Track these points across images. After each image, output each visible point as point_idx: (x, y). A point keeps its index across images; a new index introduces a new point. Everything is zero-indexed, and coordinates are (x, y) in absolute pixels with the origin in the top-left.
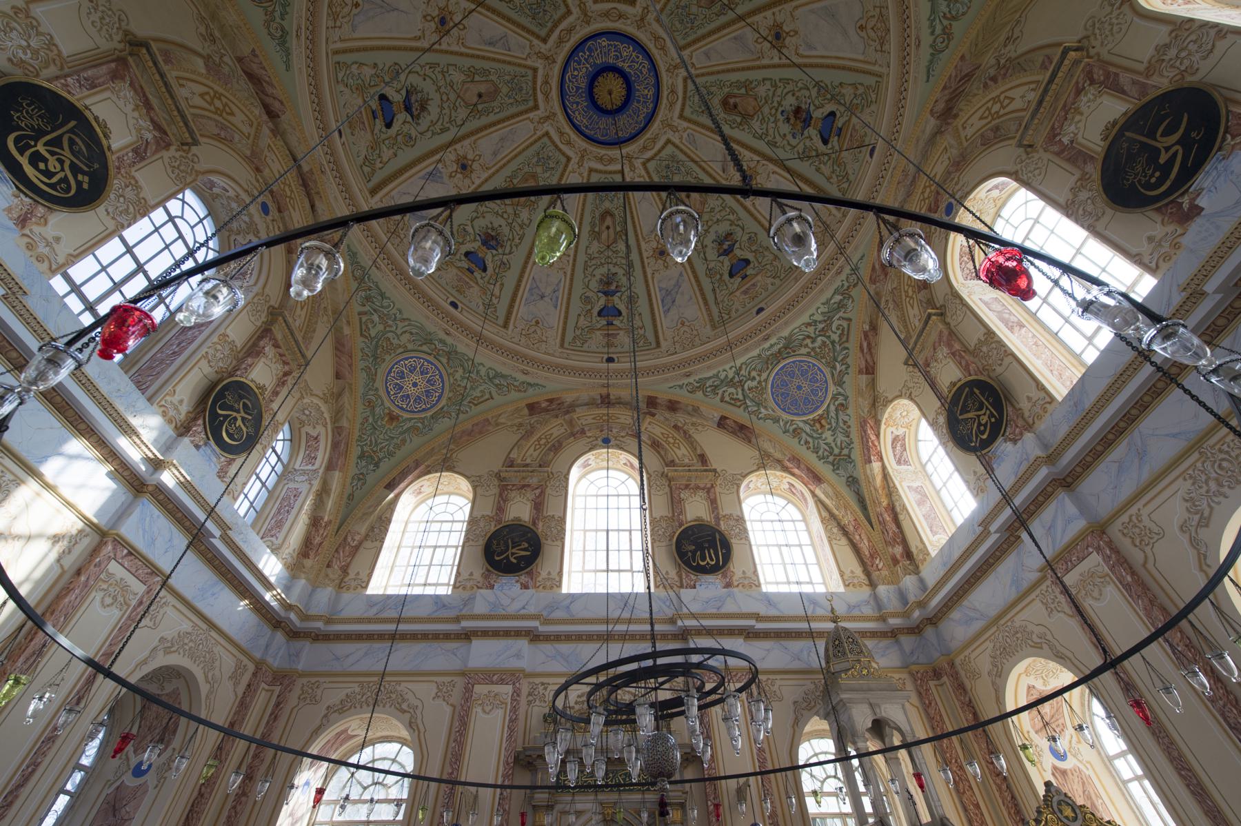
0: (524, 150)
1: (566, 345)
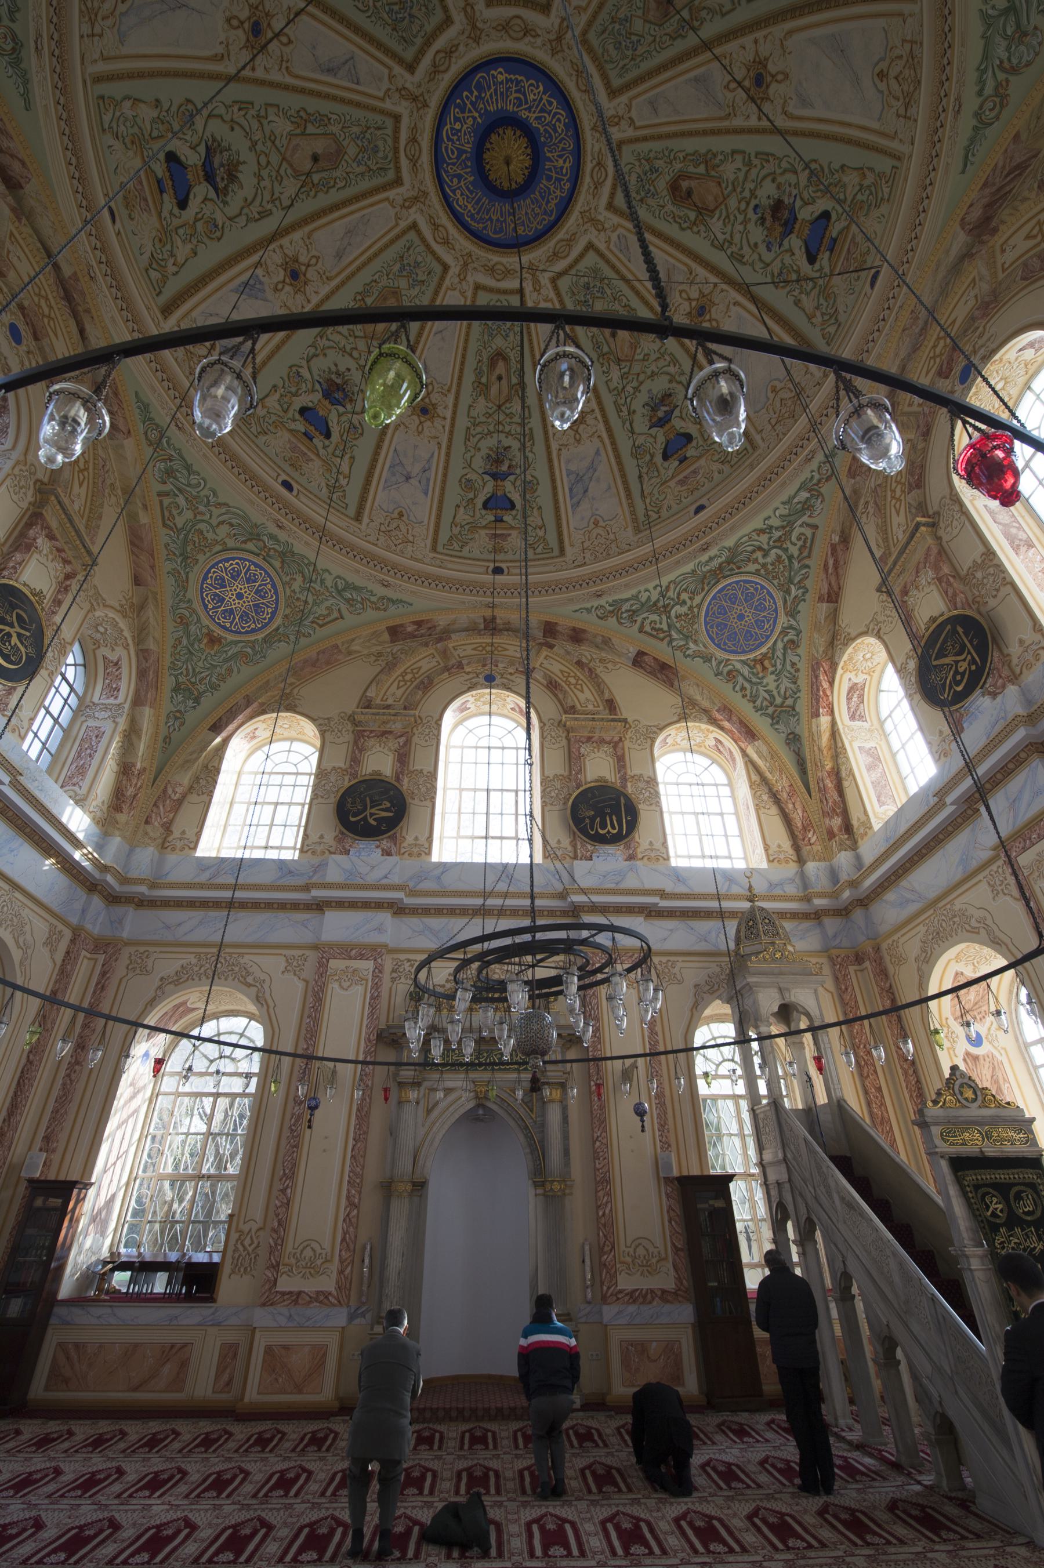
0: (381, 250)
1: (440, 548)
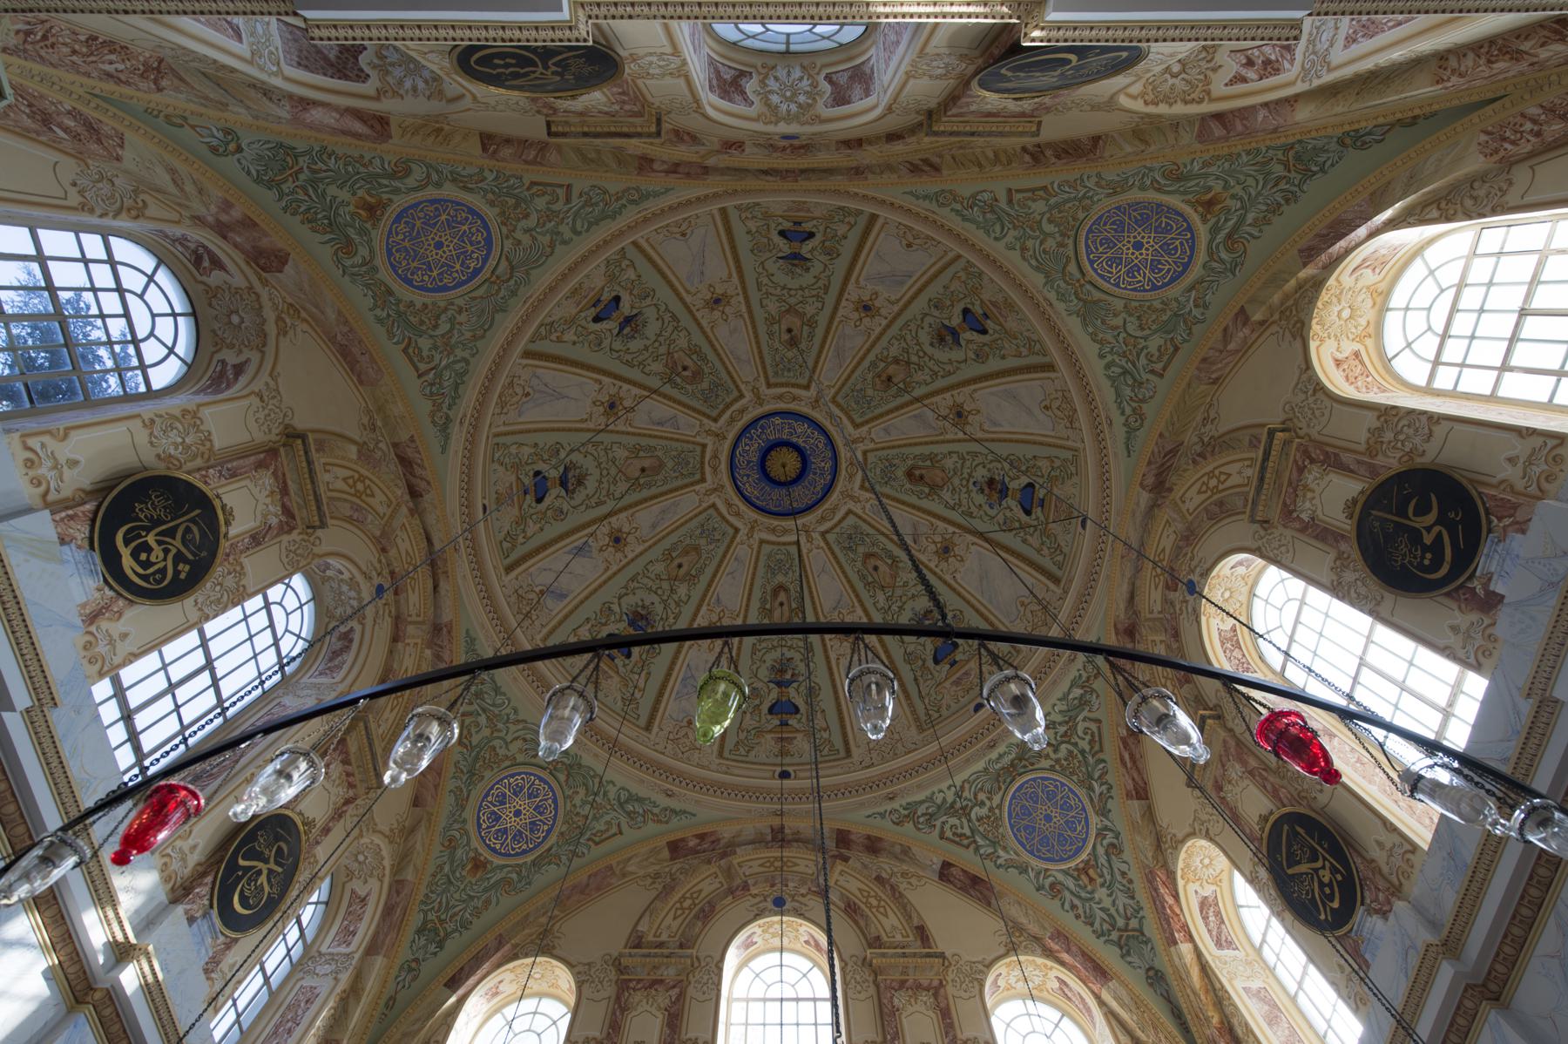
1: (726, 754)
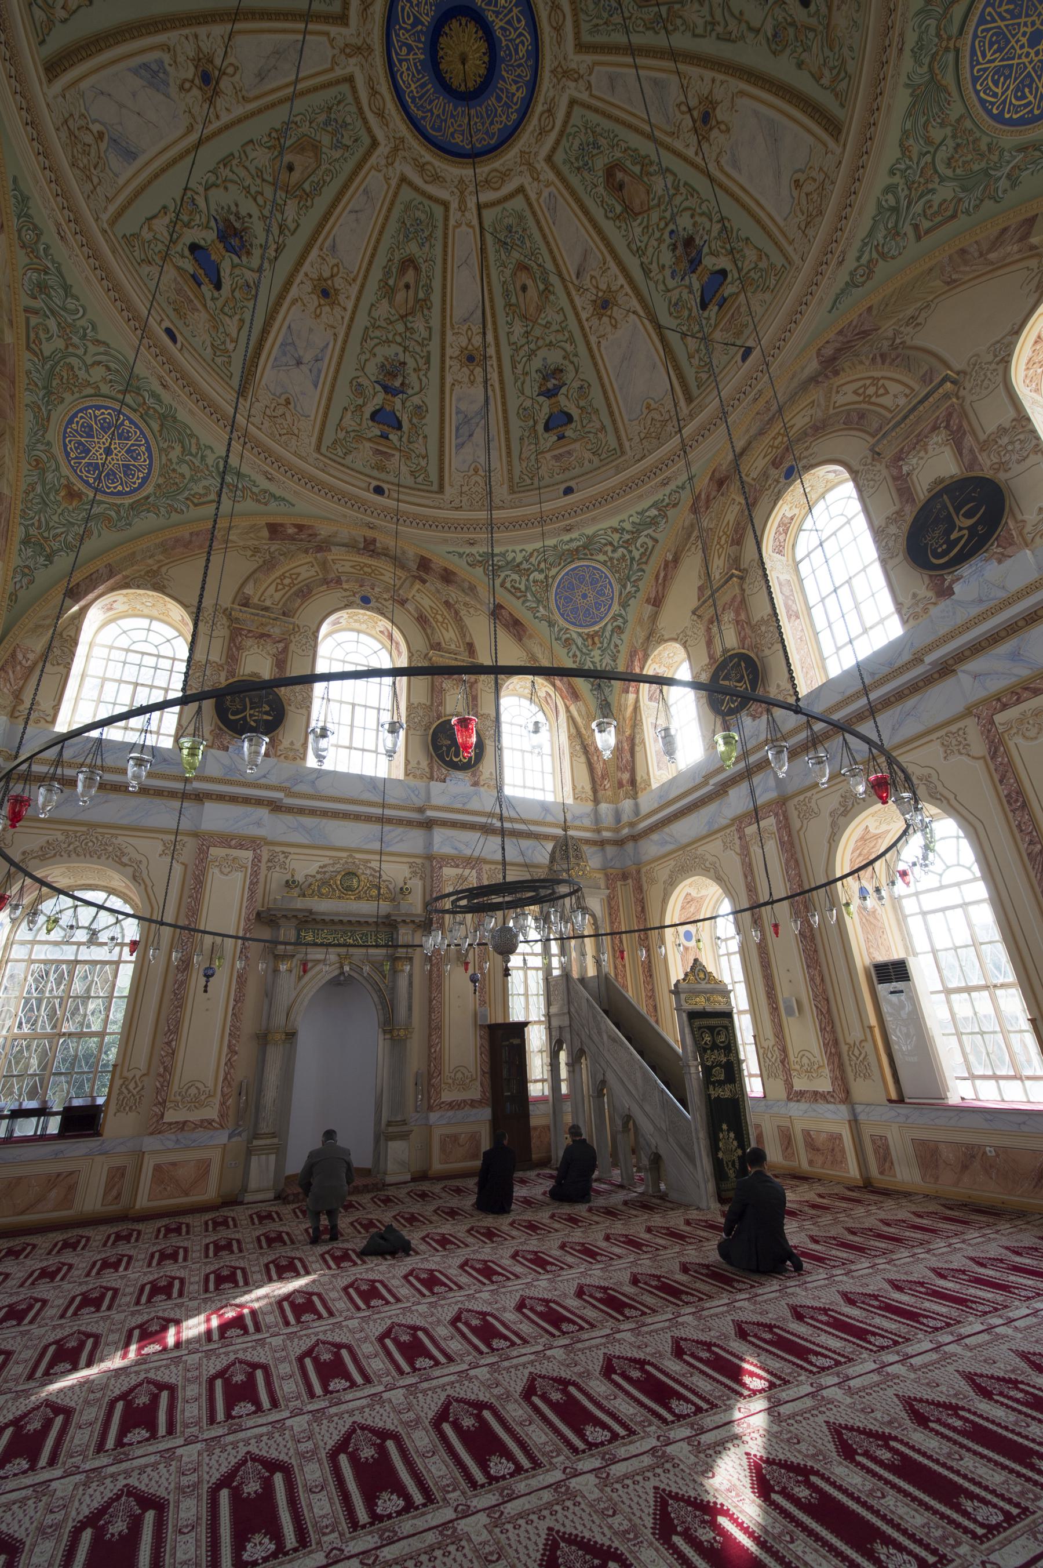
1: (323, 450)
